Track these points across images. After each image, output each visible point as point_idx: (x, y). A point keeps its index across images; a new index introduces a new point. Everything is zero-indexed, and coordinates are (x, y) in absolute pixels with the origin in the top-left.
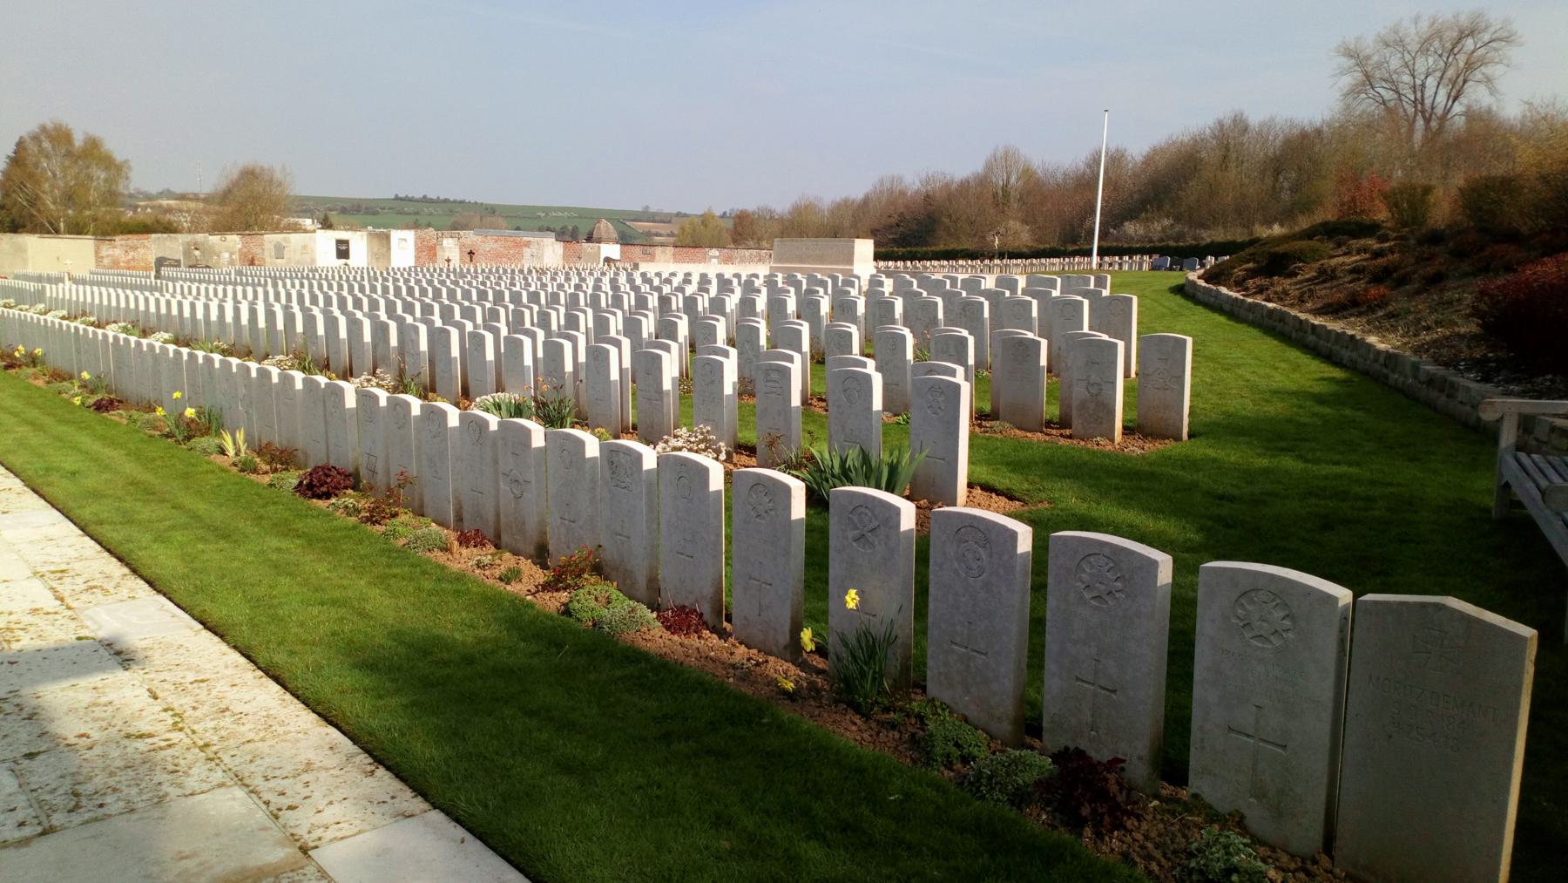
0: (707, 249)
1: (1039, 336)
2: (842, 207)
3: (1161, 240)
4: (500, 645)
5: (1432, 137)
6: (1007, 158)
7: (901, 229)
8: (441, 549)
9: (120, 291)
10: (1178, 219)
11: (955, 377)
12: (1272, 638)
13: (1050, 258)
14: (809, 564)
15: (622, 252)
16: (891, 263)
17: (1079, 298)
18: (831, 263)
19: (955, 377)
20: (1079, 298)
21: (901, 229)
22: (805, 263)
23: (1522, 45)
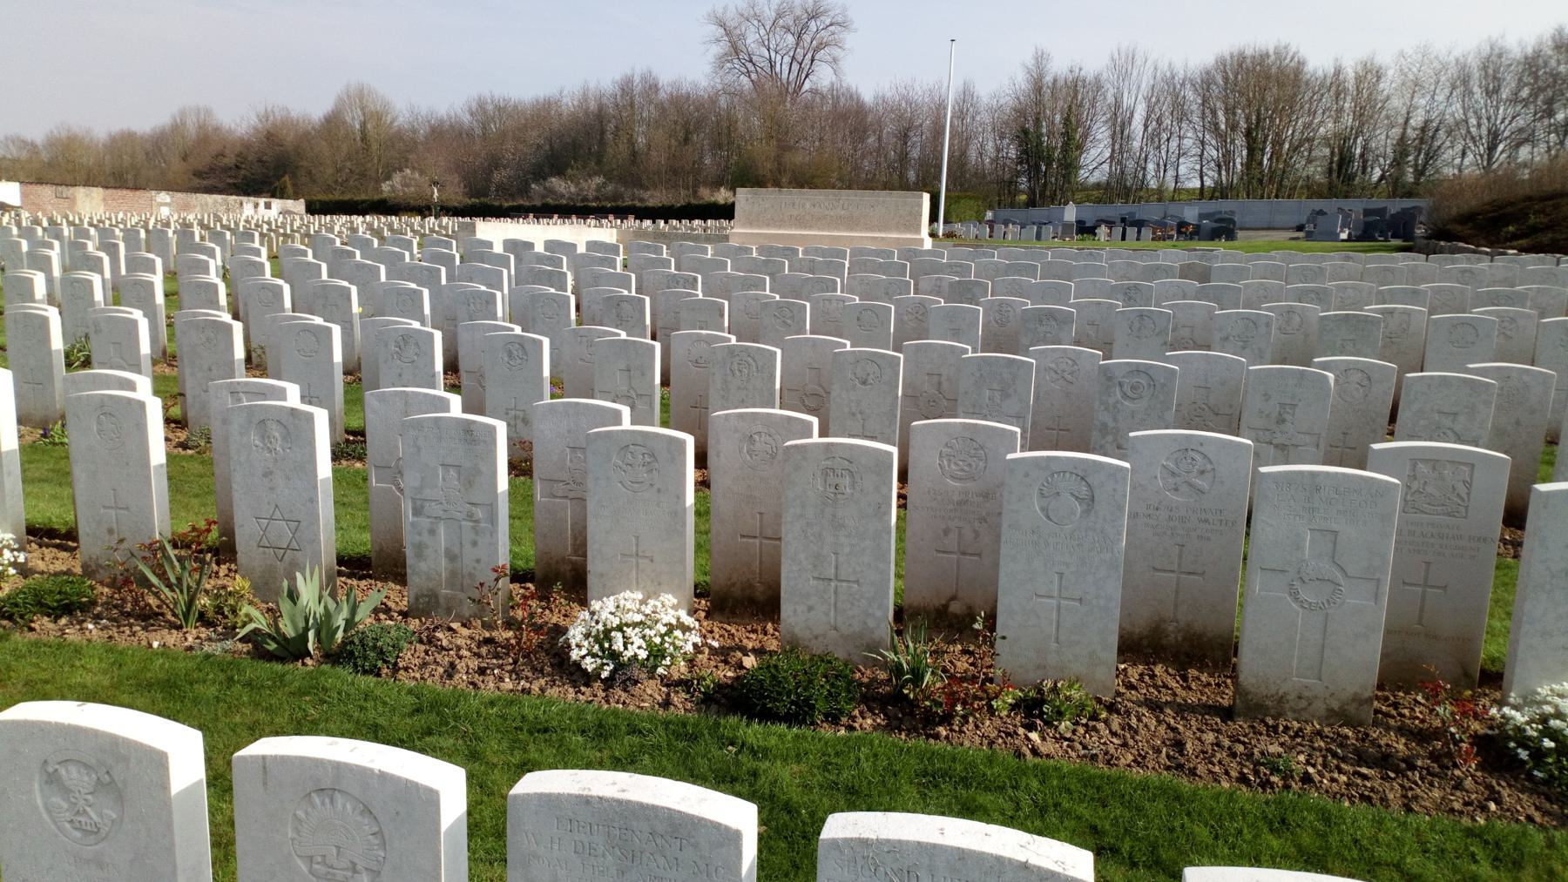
0: (153, 193)
1: (511, 322)
2: (123, 143)
3: (597, 199)
4: (609, 627)
5: (835, 106)
6: (360, 96)
7: (243, 172)
8: (55, 613)
9: (212, 225)
10: (609, 179)
11: (285, 400)
12: (1426, 241)
13: (350, 215)
14: (215, 844)
15: (24, 195)
16: (647, 223)
17: (345, 284)
18: (871, 229)
19: (285, 400)
20: (345, 284)
21: (243, 172)
22: (811, 228)
23: (856, 31)
